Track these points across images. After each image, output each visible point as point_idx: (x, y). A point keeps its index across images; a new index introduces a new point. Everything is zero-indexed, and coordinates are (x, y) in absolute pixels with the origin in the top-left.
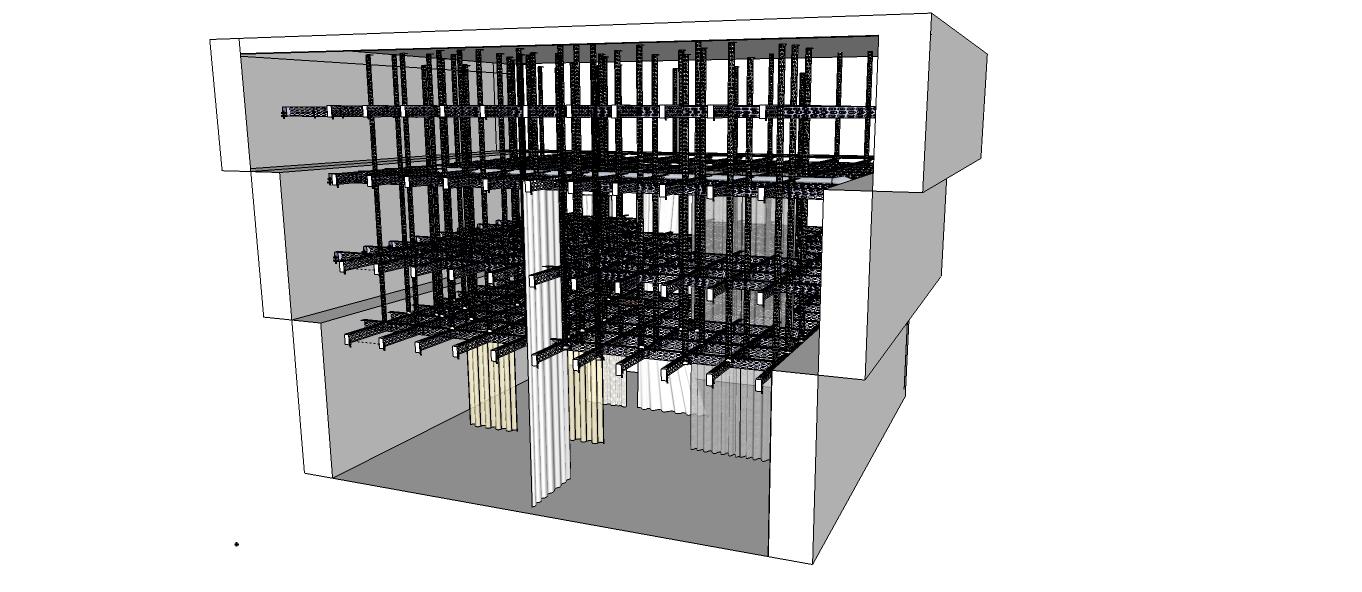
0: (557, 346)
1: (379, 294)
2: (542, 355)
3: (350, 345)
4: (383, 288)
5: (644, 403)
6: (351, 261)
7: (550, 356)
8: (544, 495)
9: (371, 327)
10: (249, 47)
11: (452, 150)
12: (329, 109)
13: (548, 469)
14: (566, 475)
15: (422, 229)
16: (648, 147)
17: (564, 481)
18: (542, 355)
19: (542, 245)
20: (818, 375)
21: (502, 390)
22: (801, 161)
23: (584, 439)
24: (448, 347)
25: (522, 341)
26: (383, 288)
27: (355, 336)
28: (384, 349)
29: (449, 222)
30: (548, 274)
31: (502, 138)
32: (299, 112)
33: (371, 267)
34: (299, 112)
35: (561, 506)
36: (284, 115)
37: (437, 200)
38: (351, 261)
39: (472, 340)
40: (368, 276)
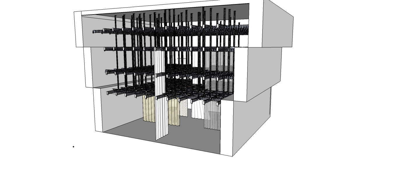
0: (163, 95)
2: (159, 97)
4: (116, 23)
5: (193, 117)
6: (109, 72)
7: (162, 97)
8: (162, 136)
9: (115, 91)
10: (83, 13)
11: (160, 24)
13: (161, 131)
14: (167, 133)
16: (232, 37)
17: (166, 134)
18: (159, 97)
20: (233, 101)
21: (152, 113)
23: (174, 125)
25: (153, 94)
26: (116, 23)
27: (109, 92)
30: (162, 74)
32: (98, 31)
33: (115, 93)
34: (98, 31)
35: (164, 140)
36: (93, 32)
37: (200, 55)
38: (109, 72)
40: (113, 76)
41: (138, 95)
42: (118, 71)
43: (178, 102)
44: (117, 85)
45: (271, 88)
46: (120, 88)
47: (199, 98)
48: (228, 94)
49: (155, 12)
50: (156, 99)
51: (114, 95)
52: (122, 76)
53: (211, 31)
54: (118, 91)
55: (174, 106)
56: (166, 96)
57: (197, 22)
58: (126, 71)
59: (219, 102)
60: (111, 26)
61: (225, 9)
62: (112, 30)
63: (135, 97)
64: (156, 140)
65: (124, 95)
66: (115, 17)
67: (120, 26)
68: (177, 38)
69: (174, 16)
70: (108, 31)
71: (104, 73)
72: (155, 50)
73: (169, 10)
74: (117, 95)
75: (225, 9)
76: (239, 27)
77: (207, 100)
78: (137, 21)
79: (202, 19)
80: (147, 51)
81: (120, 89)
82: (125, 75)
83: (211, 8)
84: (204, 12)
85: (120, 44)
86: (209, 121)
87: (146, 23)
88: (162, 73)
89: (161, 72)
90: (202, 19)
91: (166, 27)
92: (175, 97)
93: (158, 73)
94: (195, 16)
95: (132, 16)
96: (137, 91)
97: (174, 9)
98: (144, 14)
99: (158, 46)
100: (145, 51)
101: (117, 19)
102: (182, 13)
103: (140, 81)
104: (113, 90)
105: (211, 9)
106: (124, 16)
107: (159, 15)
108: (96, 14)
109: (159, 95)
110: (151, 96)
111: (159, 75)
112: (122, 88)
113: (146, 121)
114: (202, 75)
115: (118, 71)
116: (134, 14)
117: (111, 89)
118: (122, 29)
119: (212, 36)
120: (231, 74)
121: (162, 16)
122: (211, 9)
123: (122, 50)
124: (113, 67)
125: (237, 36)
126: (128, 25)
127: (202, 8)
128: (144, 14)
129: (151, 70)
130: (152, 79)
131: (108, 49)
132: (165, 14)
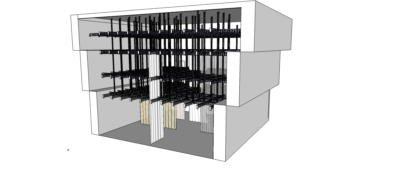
1: (113, 86)
2: (153, 101)
3: (122, 100)
4: (112, 26)
5: (191, 120)
6: (105, 75)
8: (157, 140)
10: (80, 17)
12: (108, 33)
13: (157, 134)
14: (162, 137)
15: (133, 68)
16: (221, 39)
18: (153, 101)
19: (154, 70)
20: (226, 105)
22: (136, 37)
24: (138, 100)
25: (148, 97)
26: (112, 26)
27: (105, 96)
28: (122, 100)
29: (195, 69)
30: (157, 78)
31: (204, 41)
32: (94, 35)
34: (94, 35)
35: (159, 144)
36: (90, 36)
38: (105, 75)
39: (189, 103)
41: (133, 98)
42: (114, 75)
43: (150, 103)
44: (113, 88)
45: (269, 90)
46: (116, 91)
47: (193, 102)
48: (221, 98)
49: (150, 15)
50: (162, 104)
51: (109, 98)
52: (118, 80)
53: (205, 34)
54: (114, 95)
55: (174, 109)
56: (161, 100)
57: (227, 23)
58: (123, 74)
59: (212, 107)
60: (108, 30)
61: (218, 13)
62: (117, 33)
63: (121, 99)
64: (151, 143)
65: (119, 98)
66: (112, 20)
67: (116, 29)
68: (144, 40)
69: (169, 19)
70: (103, 34)
71: (100, 76)
72: (149, 53)
73: (164, 13)
74: (122, 99)
75: (218, 13)
76: (237, 30)
77: (201, 104)
78: (146, 25)
79: (179, 23)
80: (123, 54)
81: (117, 92)
82: (130, 79)
83: (205, 12)
84: (199, 16)
85: (117, 47)
86: (205, 124)
87: (182, 25)
88: (157, 76)
89: (156, 75)
90: (179, 23)
91: (160, 31)
92: (170, 101)
93: (153, 76)
94: (190, 19)
95: (174, 19)
96: (143, 95)
97: (168, 13)
98: (139, 17)
99: (153, 50)
100: (211, 56)
101: (122, 22)
102: (177, 16)
103: (140, 83)
104: (109, 93)
105: (204, 13)
106: (120, 19)
107: (154, 18)
108: (96, 18)
109: (154, 98)
110: (157, 101)
111: (153, 79)
112: (119, 91)
113: (148, 124)
114: (184, 78)
115: (114, 75)
116: (129, 18)
117: (107, 92)
118: (127, 32)
119: (189, 39)
120: (223, 78)
121: (157, 20)
122: (204, 13)
123: (127, 53)
124: (110, 70)
125: (226, 40)
126: (125, 29)
127: (163, 14)
128: (139, 17)
129: (145, 73)
130: (148, 82)
131: (104, 52)
132: (160, 17)
